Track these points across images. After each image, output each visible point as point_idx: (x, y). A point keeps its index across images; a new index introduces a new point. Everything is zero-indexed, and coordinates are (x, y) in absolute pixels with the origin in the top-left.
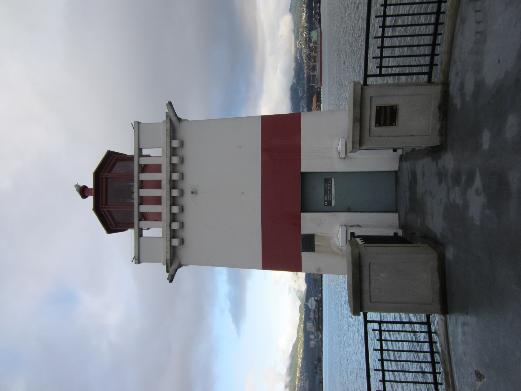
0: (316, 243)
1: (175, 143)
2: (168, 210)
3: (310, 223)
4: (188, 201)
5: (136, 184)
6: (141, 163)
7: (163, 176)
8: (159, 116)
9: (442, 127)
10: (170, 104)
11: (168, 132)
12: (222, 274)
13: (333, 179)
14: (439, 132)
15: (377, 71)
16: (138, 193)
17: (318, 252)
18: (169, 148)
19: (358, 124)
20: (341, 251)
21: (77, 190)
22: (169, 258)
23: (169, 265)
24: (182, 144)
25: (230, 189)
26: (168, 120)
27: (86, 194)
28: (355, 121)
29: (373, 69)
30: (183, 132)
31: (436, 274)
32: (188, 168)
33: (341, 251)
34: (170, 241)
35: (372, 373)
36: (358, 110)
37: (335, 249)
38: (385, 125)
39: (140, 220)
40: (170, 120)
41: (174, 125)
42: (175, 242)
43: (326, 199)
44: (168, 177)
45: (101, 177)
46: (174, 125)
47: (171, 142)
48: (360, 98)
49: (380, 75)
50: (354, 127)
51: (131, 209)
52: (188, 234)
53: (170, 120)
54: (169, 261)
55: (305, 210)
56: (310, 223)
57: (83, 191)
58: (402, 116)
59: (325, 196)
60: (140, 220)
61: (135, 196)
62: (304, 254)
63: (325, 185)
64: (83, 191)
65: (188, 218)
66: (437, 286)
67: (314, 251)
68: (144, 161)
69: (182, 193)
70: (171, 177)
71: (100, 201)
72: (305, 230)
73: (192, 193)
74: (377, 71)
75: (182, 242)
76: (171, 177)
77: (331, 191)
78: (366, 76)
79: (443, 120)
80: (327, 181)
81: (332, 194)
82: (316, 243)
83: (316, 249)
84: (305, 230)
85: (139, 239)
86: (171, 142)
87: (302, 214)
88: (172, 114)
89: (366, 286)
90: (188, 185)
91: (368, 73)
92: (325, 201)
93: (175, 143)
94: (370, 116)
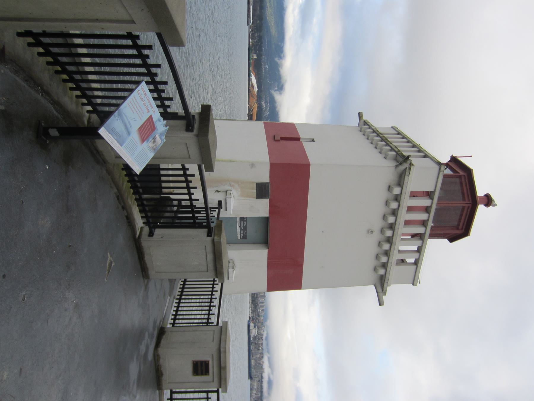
0: (255, 191)
1: (382, 272)
2: (390, 261)
3: (261, 208)
4: (377, 224)
5: (431, 224)
7: (401, 229)
8: (392, 289)
9: (158, 361)
10: (380, 304)
11: (386, 281)
13: (239, 238)
14: (160, 358)
15: (210, 395)
16: (426, 230)
17: (253, 183)
18: (388, 270)
19: (223, 365)
20: (230, 185)
21: (493, 200)
22: (406, 177)
23: (407, 170)
24: (375, 269)
25: (340, 209)
26: (385, 290)
27: (485, 197)
28: (225, 368)
30: (373, 277)
31: (149, 265)
32: (374, 250)
33: (230, 185)
36: (223, 375)
37: (237, 186)
38: (201, 362)
39: (430, 207)
40: (383, 290)
41: (381, 285)
42: (397, 190)
43: (245, 222)
44: (393, 247)
45: (471, 202)
46: (381, 285)
47: (386, 274)
48: (222, 383)
49: (207, 392)
50: (225, 363)
51: (441, 202)
52: (384, 195)
53: (383, 290)
54: (407, 173)
55: (267, 218)
56: (261, 208)
57: (488, 201)
58: (189, 369)
59: (246, 225)
60: (430, 207)
61: (429, 229)
62: (268, 181)
63: (246, 233)
64: (488, 201)
65: (381, 209)
66: (147, 258)
67: (257, 184)
69: (382, 231)
70: (391, 247)
71: (469, 211)
72: (265, 202)
73: (372, 232)
75: (390, 188)
76: (391, 247)
77: (241, 229)
78: (217, 391)
79: (158, 366)
80: (244, 237)
81: (240, 227)
82: (255, 191)
83: (255, 186)
84: (265, 202)
86: (386, 274)
87: (268, 216)
88: (381, 294)
89: (210, 257)
90: (376, 236)
92: (246, 221)
93: (382, 272)
94: (213, 368)
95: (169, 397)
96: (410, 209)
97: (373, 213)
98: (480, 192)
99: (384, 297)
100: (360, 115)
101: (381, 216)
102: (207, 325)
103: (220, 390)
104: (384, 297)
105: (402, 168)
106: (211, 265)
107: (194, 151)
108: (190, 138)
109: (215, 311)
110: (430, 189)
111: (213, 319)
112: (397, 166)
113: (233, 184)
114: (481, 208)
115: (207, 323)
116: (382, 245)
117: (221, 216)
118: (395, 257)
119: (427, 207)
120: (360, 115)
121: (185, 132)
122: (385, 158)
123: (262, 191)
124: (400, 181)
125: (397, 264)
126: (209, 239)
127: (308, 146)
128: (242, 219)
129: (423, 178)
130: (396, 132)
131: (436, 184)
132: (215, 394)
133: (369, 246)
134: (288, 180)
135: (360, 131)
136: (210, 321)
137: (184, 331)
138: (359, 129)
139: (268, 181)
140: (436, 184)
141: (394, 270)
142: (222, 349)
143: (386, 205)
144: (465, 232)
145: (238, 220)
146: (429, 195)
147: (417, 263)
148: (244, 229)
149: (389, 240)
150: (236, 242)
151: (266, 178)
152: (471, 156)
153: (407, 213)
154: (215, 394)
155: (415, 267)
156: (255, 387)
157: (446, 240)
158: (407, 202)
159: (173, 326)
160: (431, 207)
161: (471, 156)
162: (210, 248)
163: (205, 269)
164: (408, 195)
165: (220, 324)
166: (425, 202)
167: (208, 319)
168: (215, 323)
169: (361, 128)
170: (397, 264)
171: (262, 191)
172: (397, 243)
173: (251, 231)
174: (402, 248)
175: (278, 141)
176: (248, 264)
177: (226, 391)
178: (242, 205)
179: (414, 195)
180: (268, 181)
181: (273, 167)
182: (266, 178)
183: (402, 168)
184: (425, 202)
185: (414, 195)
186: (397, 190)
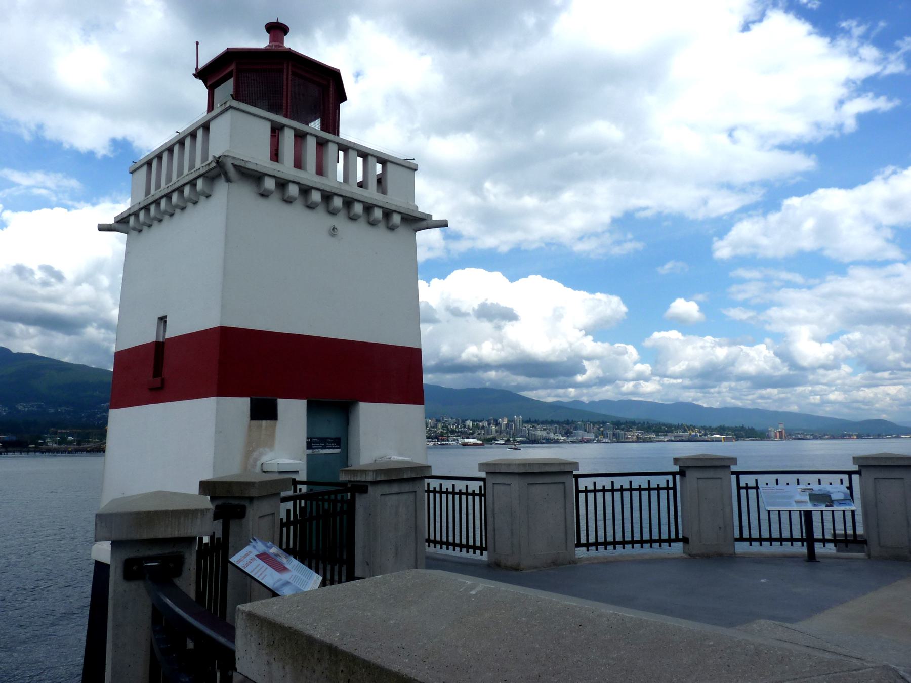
0: (264, 423)
1: (396, 219)
2: (318, 186)
3: (293, 412)
4: (320, 220)
6: (309, 137)
7: (308, 176)
12: (430, 293)
15: (742, 484)
17: (250, 426)
24: (392, 228)
29: (744, 480)
30: (403, 232)
34: (274, 177)
35: (610, 479)
37: (255, 454)
46: (417, 221)
49: (578, 492)
52: (273, 206)
54: (242, 164)
56: (293, 412)
57: (277, 29)
59: (318, 438)
63: (331, 438)
65: (297, 212)
68: (332, 148)
69: (333, 213)
70: (359, 201)
74: (742, 484)
75: (264, 195)
76: (359, 201)
77: (324, 448)
78: (577, 477)
82: (264, 422)
85: (337, 143)
89: (395, 488)
90: (340, 222)
91: (741, 476)
95: (584, 549)
96: (298, 164)
97: (305, 226)
98: (262, 42)
99: (434, 218)
100: (103, 228)
101: (262, 202)
102: (485, 495)
103: (575, 472)
104: (434, 218)
105: (232, 172)
106: (407, 487)
107: (265, 507)
108: (254, 512)
109: (460, 486)
110: (267, 127)
111: (475, 486)
112: (228, 180)
113: (251, 461)
114: (292, 43)
115: (480, 495)
116: (265, 190)
117: (305, 479)
118: (371, 194)
119: (295, 136)
120: (103, 228)
121: (244, 520)
122: (208, 196)
123: (264, 411)
124: (253, 177)
125: (384, 192)
126: (371, 489)
127: (173, 331)
128: (309, 446)
129: (245, 135)
130: (145, 168)
131: (260, 117)
132: (580, 480)
133: (357, 236)
134: (242, 365)
135: (140, 231)
136: (477, 492)
137: (494, 530)
138: (134, 233)
139: (247, 400)
140: (260, 117)
141: (392, 199)
142: (522, 470)
143: (291, 202)
144: (334, 76)
145: (310, 451)
146: (276, 130)
147: (384, 161)
148: (324, 442)
149: (327, 197)
150: (345, 458)
151: (243, 404)
152: (197, 43)
153: (282, 163)
154: (580, 480)
155: (389, 165)
156: (544, 433)
157: (343, 106)
158: (286, 168)
159: (486, 549)
160: (295, 130)
161: (197, 43)
162: (386, 489)
163: (412, 496)
164: (275, 165)
165: (483, 474)
166: (288, 139)
167: (474, 494)
168: (482, 483)
169: (134, 229)
170: (384, 192)
171: (264, 411)
172: (332, 184)
173: (328, 429)
174: (340, 177)
175: (163, 381)
176: (384, 434)
177: (577, 464)
178: (287, 446)
179: (275, 156)
180: (247, 400)
181: (224, 390)
182: (243, 404)
183: (232, 172)
184: (288, 139)
185: (275, 156)
186: (269, 184)
